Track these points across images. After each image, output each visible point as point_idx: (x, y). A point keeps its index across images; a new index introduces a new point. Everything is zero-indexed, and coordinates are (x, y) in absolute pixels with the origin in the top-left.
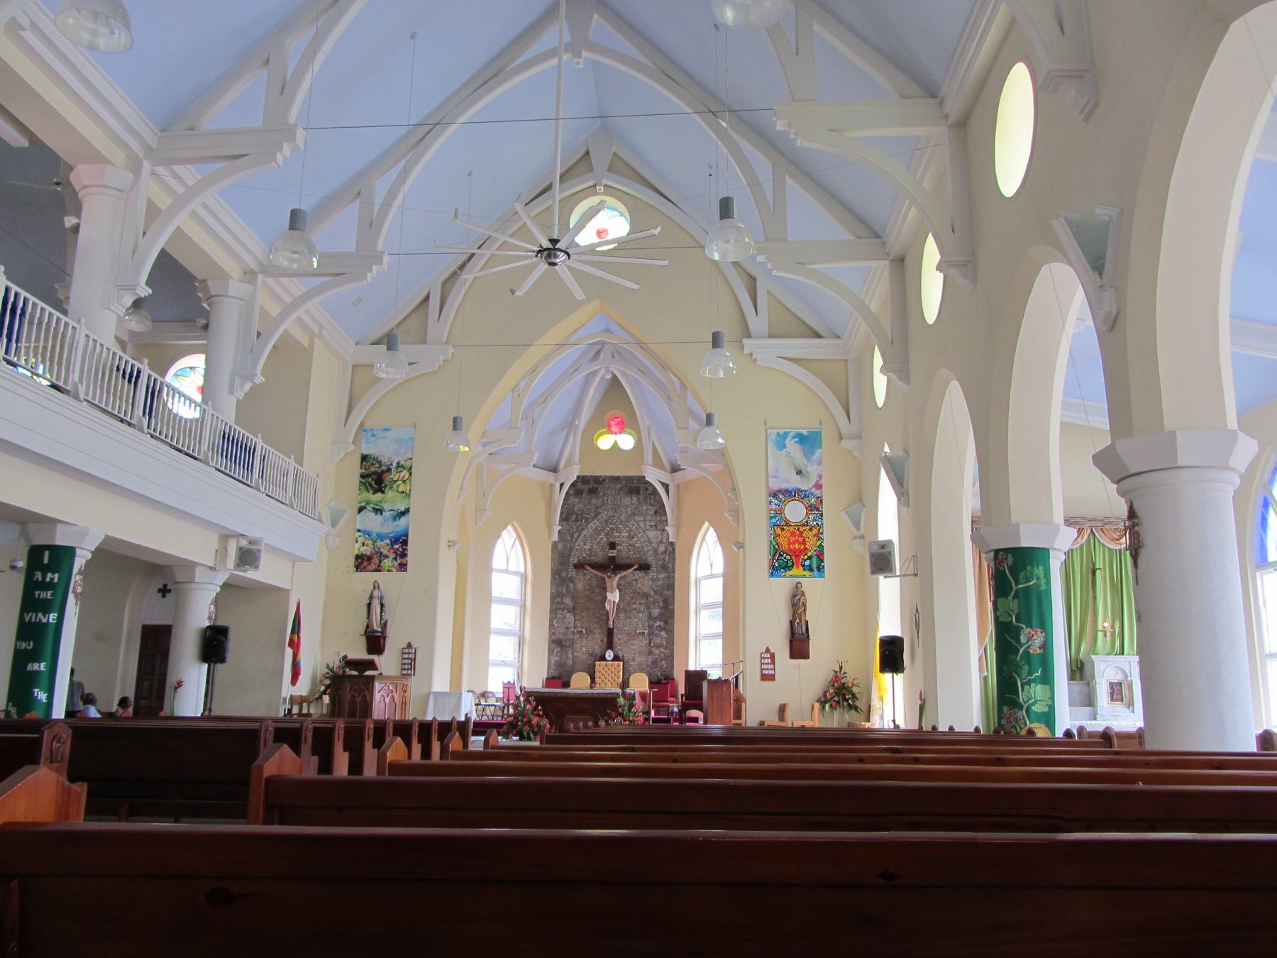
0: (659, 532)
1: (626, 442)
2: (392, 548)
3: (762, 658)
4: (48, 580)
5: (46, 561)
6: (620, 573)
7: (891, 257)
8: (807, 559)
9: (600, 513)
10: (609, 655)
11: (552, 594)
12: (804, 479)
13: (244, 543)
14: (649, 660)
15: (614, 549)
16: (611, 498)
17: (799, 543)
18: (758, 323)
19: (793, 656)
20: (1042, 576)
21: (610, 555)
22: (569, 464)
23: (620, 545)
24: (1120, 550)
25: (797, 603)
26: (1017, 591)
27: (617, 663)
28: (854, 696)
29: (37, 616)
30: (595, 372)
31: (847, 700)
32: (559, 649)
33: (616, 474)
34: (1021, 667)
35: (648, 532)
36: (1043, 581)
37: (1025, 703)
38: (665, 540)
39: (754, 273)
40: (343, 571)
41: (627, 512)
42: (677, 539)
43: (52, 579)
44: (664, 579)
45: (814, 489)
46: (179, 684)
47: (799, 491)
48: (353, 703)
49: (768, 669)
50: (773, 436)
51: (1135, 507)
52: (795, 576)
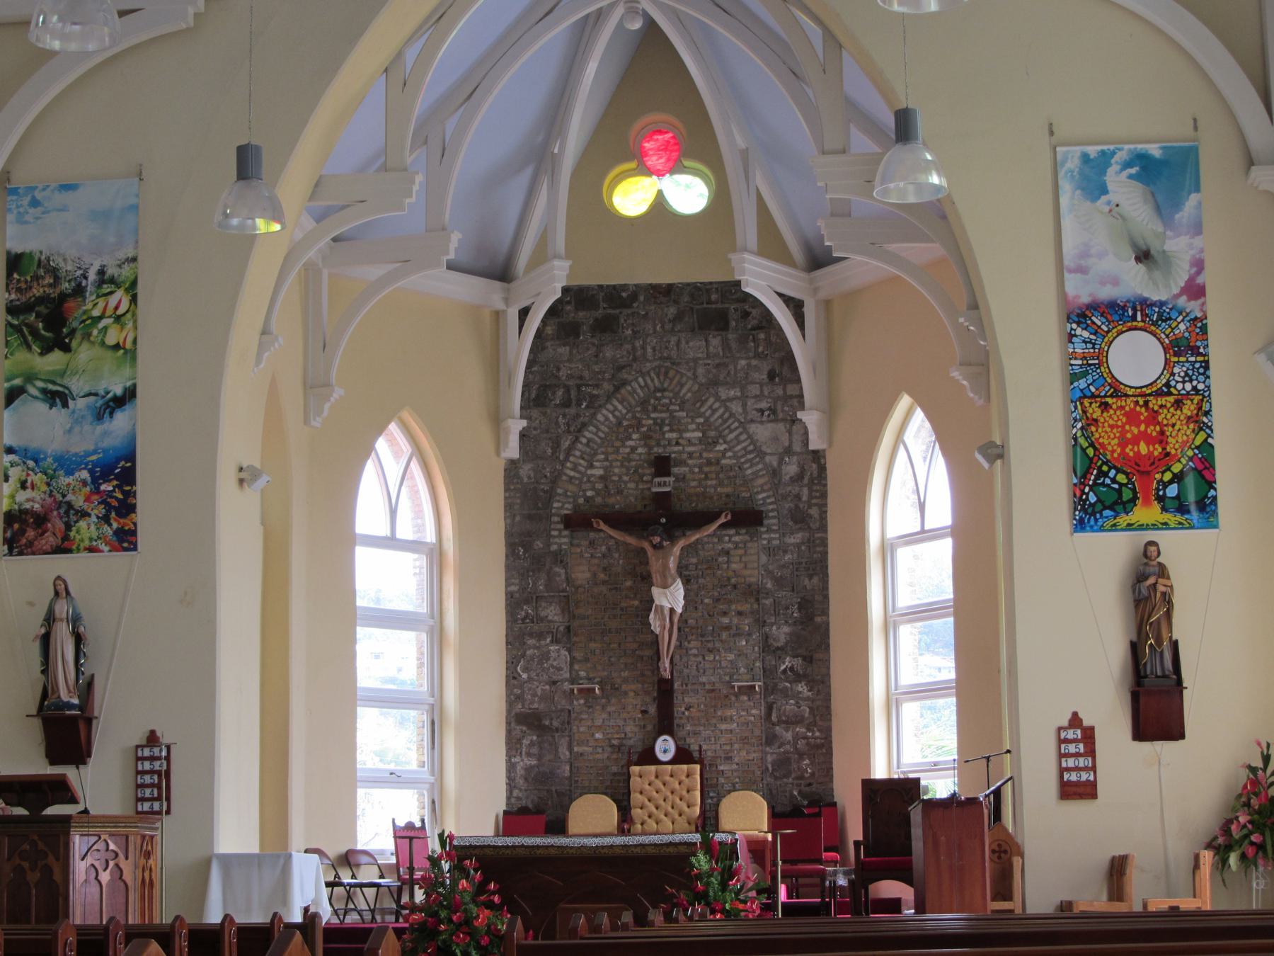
0: (781, 427)
3: (1061, 741)
8: (1171, 482)
9: (624, 383)
10: (665, 747)
11: (510, 596)
14: (769, 758)
15: (668, 474)
16: (653, 341)
17: (1150, 440)
21: (655, 490)
22: (541, 255)
23: (683, 463)
27: (685, 767)
30: (600, 15)
35: (753, 428)
38: (797, 447)
41: (695, 377)
42: (830, 444)
44: (798, 546)
45: (1184, 298)
47: (1145, 304)
49: (1077, 769)
50: (1073, 164)
52: (1142, 527)
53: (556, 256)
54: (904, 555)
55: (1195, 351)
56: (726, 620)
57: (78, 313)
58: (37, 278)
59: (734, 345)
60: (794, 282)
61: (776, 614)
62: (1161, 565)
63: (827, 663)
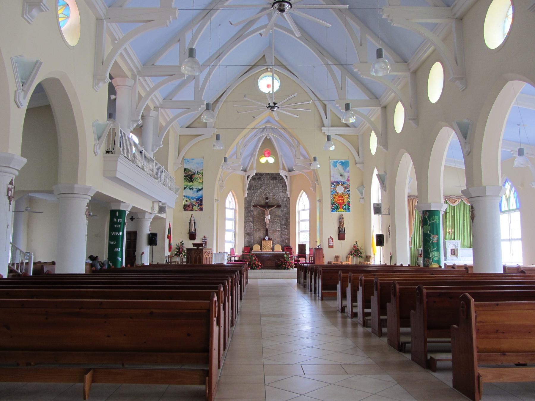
0: (284, 194)
1: (271, 160)
2: (197, 202)
3: (329, 240)
4: (119, 221)
5: (117, 215)
6: (270, 208)
7: (382, 106)
9: (262, 187)
10: (267, 238)
11: (245, 216)
12: (343, 178)
13: (160, 204)
14: (281, 240)
15: (268, 200)
16: (266, 181)
17: (342, 200)
18: (327, 122)
19: (340, 239)
20: (437, 219)
22: (252, 168)
23: (270, 198)
24: (455, 206)
25: (341, 221)
26: (430, 224)
28: (361, 253)
29: (116, 233)
30: (265, 135)
31: (359, 254)
32: (248, 236)
33: (268, 172)
34: (431, 247)
36: (438, 221)
37: (432, 257)
38: (286, 196)
39: (326, 102)
40: (179, 211)
41: (272, 186)
42: (291, 196)
43: (120, 221)
44: (286, 210)
45: (347, 181)
46: (143, 253)
47: (341, 182)
48: (196, 259)
49: (331, 244)
50: (332, 162)
51: (473, 206)
52: (340, 212)
53: (254, 169)
54: (301, 212)
55: (348, 188)
56: (275, 220)
57: (194, 177)
58: (188, 172)
59: (277, 182)
60: (286, 173)
61: (283, 220)
62: (343, 217)
63: (289, 227)
